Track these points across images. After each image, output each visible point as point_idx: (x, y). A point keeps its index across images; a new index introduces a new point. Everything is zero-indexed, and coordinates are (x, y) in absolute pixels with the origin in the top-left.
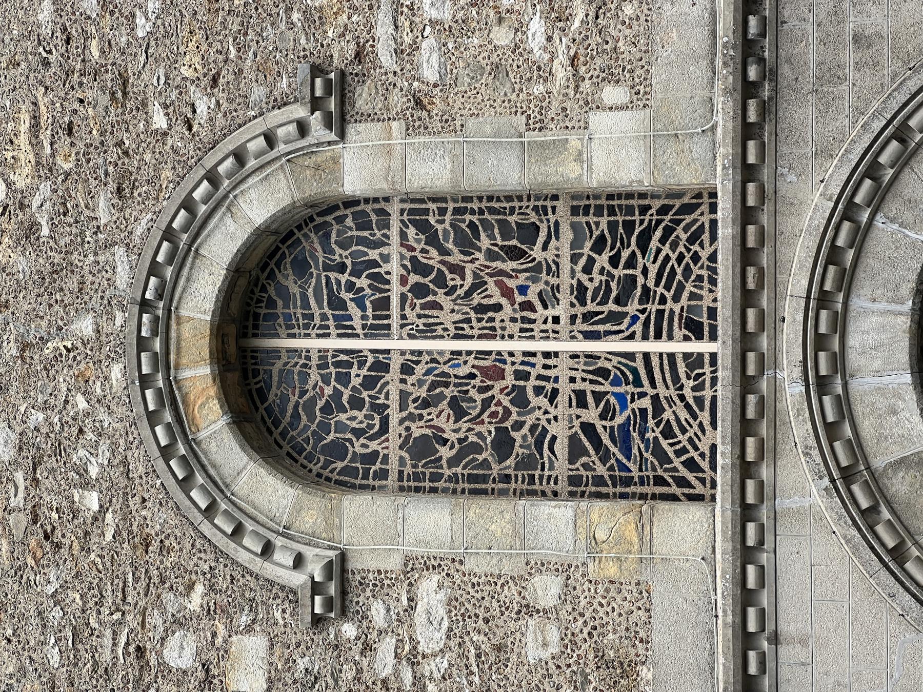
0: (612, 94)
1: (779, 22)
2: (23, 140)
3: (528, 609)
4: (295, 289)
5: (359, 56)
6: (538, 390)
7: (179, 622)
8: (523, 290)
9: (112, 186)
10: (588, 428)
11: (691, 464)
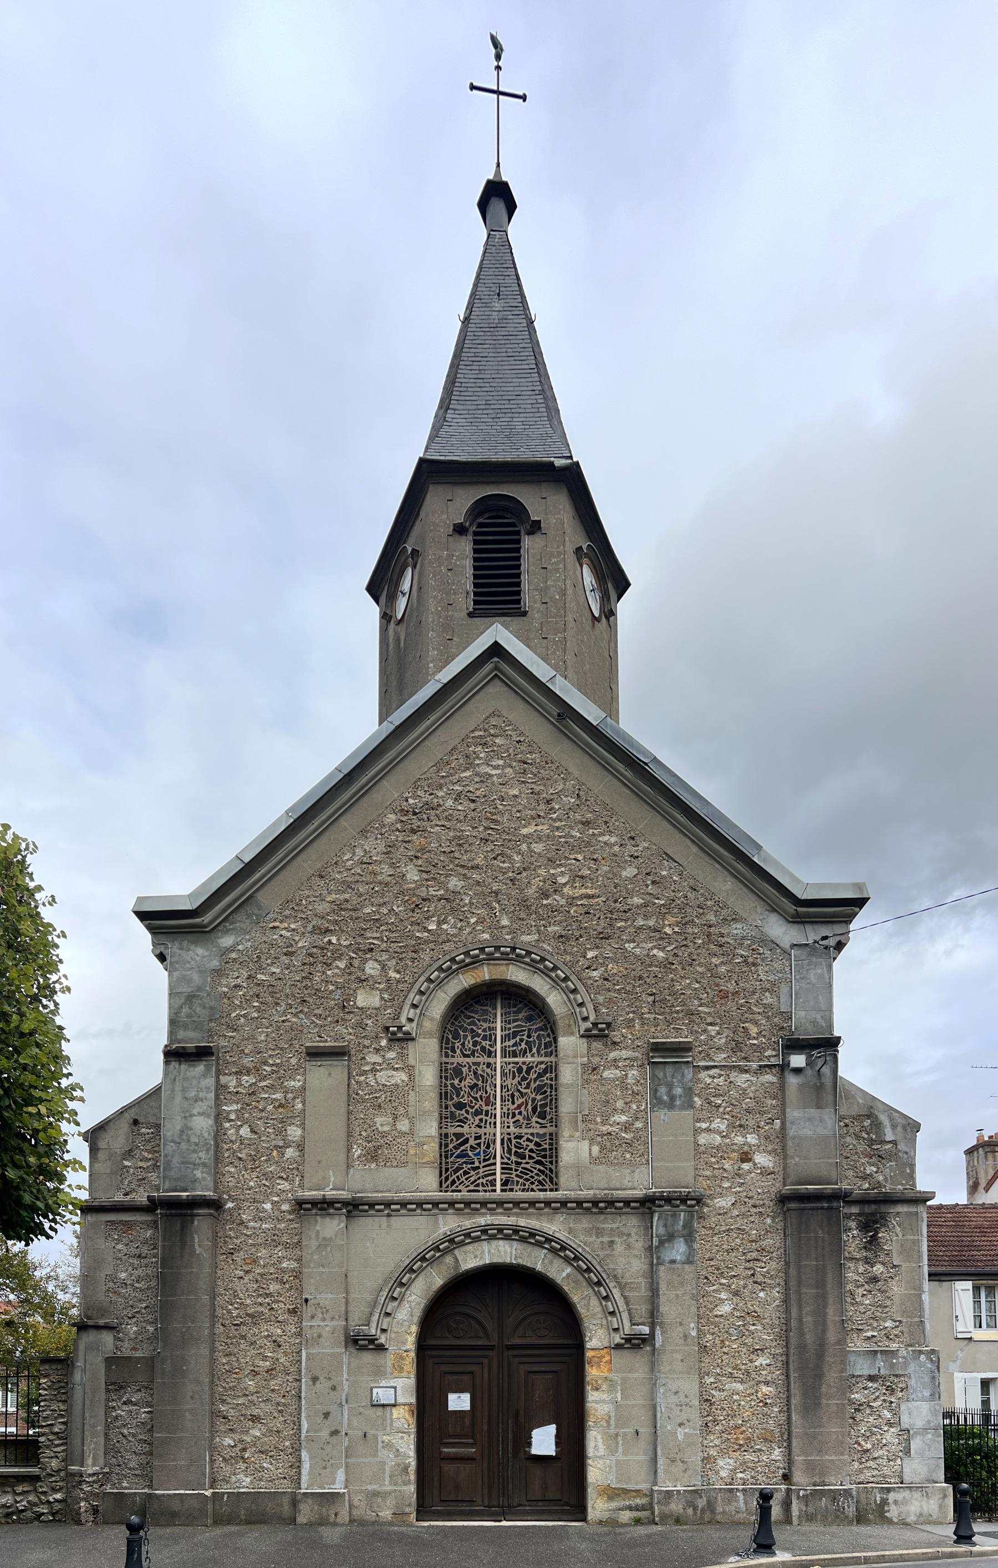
0: (596, 1149)
1: (620, 1214)
2: (583, 891)
3: (395, 1118)
4: (521, 1016)
6: (481, 1120)
7: (384, 967)
8: (520, 1113)
9: (563, 933)
10: (467, 1141)
11: (453, 1182)
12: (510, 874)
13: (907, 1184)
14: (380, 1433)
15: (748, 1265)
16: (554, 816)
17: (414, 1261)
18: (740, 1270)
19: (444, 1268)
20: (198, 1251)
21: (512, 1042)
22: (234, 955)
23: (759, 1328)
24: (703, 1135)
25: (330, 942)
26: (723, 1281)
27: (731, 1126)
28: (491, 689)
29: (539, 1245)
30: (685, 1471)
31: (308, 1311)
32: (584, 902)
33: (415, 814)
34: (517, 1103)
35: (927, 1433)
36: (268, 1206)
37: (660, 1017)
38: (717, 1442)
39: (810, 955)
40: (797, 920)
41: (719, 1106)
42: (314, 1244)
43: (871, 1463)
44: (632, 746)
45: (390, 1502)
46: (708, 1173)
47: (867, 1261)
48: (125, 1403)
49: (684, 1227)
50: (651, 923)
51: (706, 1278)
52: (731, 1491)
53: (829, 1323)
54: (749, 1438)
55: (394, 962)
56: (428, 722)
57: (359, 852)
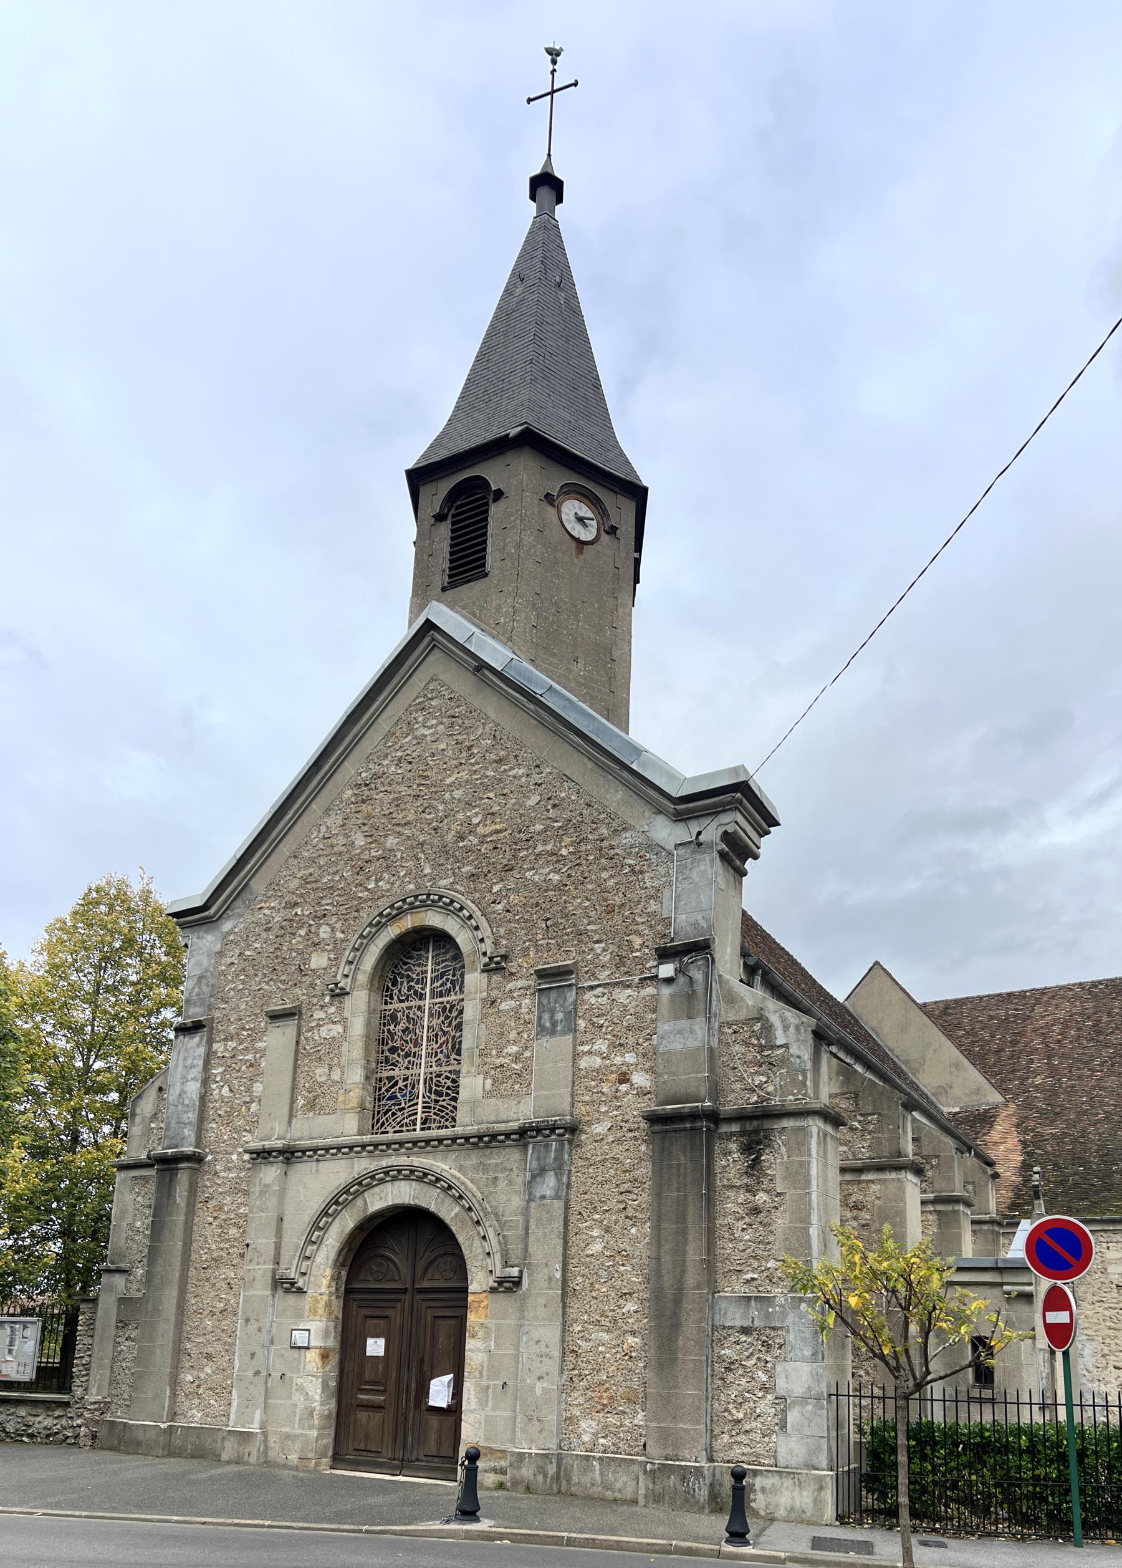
0: (489, 1082)
1: (504, 1147)
2: (493, 827)
3: (331, 1069)
4: (448, 956)
5: (512, 974)
6: (409, 1062)
7: (333, 929)
8: (442, 1052)
9: (474, 871)
10: (396, 1083)
11: (383, 1124)
12: (434, 824)
13: (799, 1092)
14: (295, 1376)
15: (621, 1198)
16: (473, 761)
17: (328, 1205)
18: (613, 1204)
19: (356, 1210)
20: (178, 1200)
21: (440, 982)
22: (231, 937)
23: (629, 1268)
24: (585, 1058)
25: (296, 914)
26: (596, 1216)
27: (612, 1045)
28: (431, 658)
29: (432, 1184)
30: (541, 1432)
31: (249, 1254)
32: (494, 838)
33: (367, 785)
34: (440, 1042)
35: (807, 1404)
36: (234, 1157)
37: (553, 942)
38: (581, 1400)
39: (694, 852)
40: (680, 817)
41: (602, 1026)
42: (257, 1190)
43: (742, 1438)
44: (530, 681)
45: (298, 1446)
46: (587, 1098)
47: (748, 1189)
48: (127, 1339)
49: (555, 1159)
50: (549, 847)
51: (580, 1213)
52: (587, 1458)
53: (689, 1264)
54: (611, 1398)
55: (340, 923)
56: (377, 703)
57: (323, 829)
